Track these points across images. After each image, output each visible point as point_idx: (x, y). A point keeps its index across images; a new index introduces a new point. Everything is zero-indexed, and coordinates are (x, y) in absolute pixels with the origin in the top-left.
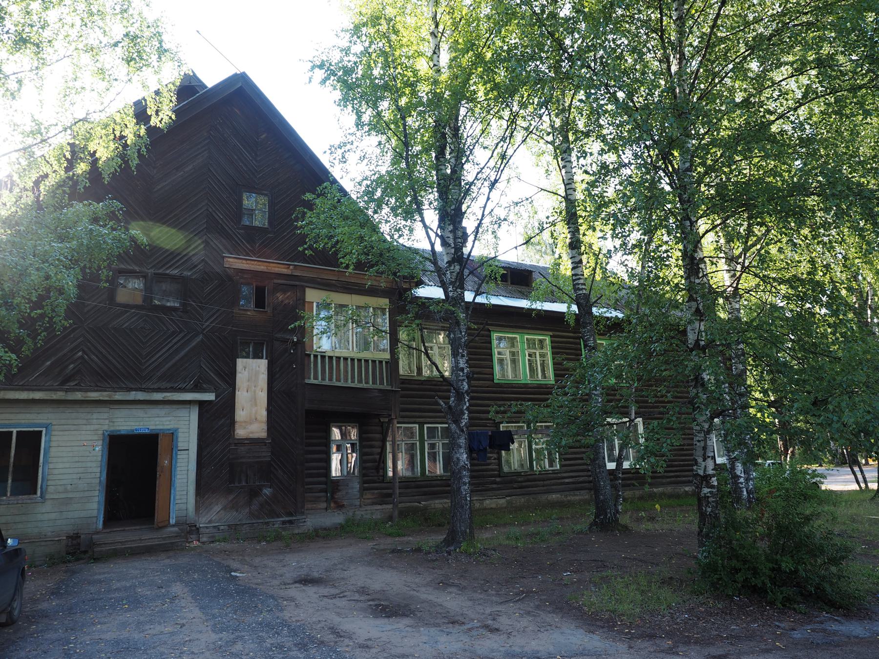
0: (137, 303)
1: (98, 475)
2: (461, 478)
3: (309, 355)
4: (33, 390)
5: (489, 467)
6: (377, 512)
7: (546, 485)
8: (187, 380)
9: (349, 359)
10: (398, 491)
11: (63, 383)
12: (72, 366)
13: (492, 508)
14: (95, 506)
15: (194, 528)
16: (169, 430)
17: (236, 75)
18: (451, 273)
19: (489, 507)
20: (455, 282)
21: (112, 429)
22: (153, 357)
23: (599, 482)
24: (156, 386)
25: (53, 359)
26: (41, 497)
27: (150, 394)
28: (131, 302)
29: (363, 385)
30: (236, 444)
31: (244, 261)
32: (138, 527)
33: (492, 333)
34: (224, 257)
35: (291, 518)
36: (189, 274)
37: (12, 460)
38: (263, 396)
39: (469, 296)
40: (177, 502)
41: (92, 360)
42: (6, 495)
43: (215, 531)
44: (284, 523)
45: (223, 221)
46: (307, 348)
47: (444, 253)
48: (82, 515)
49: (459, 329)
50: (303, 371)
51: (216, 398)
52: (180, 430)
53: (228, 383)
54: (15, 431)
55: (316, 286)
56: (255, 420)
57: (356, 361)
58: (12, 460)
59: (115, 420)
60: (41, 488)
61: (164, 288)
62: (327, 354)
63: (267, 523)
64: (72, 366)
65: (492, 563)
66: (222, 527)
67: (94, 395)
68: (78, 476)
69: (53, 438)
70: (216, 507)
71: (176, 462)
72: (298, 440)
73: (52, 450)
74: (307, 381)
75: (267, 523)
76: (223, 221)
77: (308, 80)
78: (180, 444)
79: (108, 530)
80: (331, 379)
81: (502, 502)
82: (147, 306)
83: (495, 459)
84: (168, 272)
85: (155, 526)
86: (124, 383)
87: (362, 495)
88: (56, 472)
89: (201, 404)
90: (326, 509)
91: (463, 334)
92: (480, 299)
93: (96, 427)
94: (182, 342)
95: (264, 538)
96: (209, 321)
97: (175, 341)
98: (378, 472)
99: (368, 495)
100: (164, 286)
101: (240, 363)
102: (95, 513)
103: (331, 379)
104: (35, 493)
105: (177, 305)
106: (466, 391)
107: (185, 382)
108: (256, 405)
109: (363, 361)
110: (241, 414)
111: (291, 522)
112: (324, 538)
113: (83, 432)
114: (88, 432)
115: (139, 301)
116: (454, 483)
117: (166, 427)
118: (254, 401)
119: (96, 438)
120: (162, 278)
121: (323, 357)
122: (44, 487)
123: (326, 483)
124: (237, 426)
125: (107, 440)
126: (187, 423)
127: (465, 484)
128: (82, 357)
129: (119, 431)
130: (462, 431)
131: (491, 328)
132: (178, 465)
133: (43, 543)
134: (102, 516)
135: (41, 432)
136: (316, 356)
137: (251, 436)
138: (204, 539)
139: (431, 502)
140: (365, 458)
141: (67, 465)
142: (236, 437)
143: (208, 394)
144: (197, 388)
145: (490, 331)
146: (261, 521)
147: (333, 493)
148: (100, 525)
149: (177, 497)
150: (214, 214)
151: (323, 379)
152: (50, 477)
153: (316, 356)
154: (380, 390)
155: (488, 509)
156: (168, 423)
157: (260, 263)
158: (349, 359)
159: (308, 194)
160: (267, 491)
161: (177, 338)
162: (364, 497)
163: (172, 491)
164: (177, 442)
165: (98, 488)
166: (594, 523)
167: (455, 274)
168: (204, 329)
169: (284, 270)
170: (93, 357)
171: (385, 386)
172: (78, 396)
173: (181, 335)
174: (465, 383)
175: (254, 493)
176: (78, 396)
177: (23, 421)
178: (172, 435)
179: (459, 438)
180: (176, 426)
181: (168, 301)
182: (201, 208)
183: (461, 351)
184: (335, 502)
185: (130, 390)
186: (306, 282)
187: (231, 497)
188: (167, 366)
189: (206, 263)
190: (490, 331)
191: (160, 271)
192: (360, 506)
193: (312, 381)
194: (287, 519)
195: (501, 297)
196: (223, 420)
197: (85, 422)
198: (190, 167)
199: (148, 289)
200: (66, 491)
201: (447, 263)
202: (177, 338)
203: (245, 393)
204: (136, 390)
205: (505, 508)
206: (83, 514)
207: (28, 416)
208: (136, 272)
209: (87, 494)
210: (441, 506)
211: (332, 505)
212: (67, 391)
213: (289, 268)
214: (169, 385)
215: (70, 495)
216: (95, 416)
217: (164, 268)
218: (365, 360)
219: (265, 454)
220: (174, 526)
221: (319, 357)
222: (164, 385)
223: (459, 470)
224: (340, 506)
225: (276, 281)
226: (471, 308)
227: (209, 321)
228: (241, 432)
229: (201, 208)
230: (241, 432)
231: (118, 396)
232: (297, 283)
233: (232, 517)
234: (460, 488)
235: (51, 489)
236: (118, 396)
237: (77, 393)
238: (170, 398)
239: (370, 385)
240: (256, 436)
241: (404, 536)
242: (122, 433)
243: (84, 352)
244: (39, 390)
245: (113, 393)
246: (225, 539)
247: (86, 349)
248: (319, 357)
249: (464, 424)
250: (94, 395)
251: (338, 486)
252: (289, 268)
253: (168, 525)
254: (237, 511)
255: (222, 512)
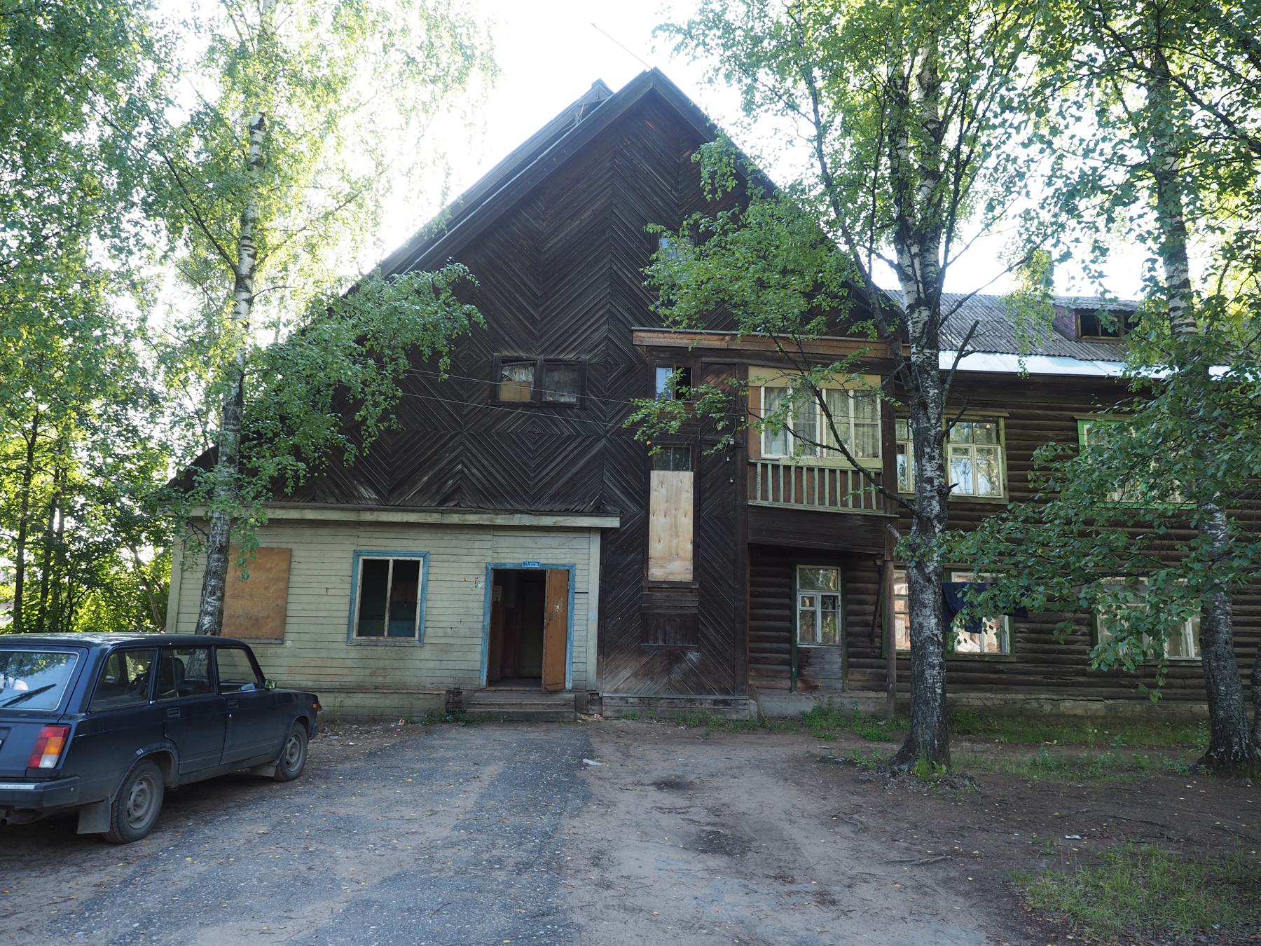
0: (524, 400)
1: (481, 618)
2: (924, 656)
3: (755, 465)
4: (407, 511)
5: (1072, 647)
6: (867, 702)
7: (1190, 687)
8: (587, 500)
9: (816, 470)
10: (894, 673)
11: (442, 503)
12: (450, 482)
13: (1075, 716)
14: (478, 657)
15: (596, 697)
16: (563, 565)
17: (644, 74)
18: (914, 323)
19: (1070, 712)
20: (921, 337)
21: (497, 561)
22: (543, 470)
23: (1217, 685)
24: (547, 508)
25: (431, 474)
26: (420, 640)
27: (537, 518)
28: (517, 399)
29: (838, 509)
30: (650, 589)
31: (660, 335)
32: (527, 689)
33: (1080, 424)
34: (633, 331)
35: (726, 697)
36: (588, 357)
37: (389, 594)
38: (687, 523)
39: (946, 360)
40: (574, 660)
41: (473, 474)
42: (383, 635)
43: (622, 703)
44: (716, 702)
45: (632, 281)
46: (751, 453)
47: (904, 293)
48: (463, 667)
49: (926, 414)
50: (743, 490)
51: (622, 524)
52: (577, 567)
53: (640, 505)
54: (391, 559)
55: (763, 363)
56: (676, 556)
57: (827, 472)
58: (389, 594)
59: (499, 551)
60: (420, 630)
61: (557, 379)
62: (780, 463)
63: (692, 701)
64: (450, 482)
65: (953, 800)
66: (631, 700)
67: (473, 519)
68: (459, 618)
69: (432, 571)
70: (625, 672)
71: (573, 608)
72: (737, 586)
73: (431, 584)
74: (751, 502)
75: (692, 701)
76: (632, 281)
77: (650, 50)
78: (577, 585)
79: (493, 689)
80: (787, 500)
81: (1097, 707)
82: (538, 404)
83: (1084, 634)
84: (561, 357)
85: (542, 688)
86: (508, 502)
87: (845, 675)
88: (435, 611)
89: (604, 532)
90: (790, 690)
91: (933, 422)
92: (968, 364)
93: (478, 558)
94: (579, 449)
95: (685, 720)
96: (614, 421)
97: (569, 449)
98: (872, 641)
99: (857, 676)
100: (557, 376)
101: (655, 476)
102: (477, 665)
103: (787, 500)
104: (414, 636)
105: (573, 400)
106: (937, 516)
107: (584, 503)
108: (677, 536)
109: (838, 472)
110: (656, 548)
111: (725, 703)
112: (771, 731)
113: (464, 565)
114: (469, 565)
115: (527, 398)
116: (914, 663)
117: (560, 562)
118: (675, 529)
119: (478, 572)
120: (553, 365)
121: (775, 467)
122: (422, 629)
123: (790, 653)
124: (651, 562)
125: (491, 575)
126: (586, 557)
127: (932, 666)
128: (461, 471)
129: (505, 564)
130: (929, 580)
131: (1076, 415)
132: (576, 612)
133: (421, 696)
134: (485, 670)
135: (419, 562)
136: (765, 466)
137: (671, 578)
138: (609, 713)
139: (962, 695)
140: (851, 618)
141: (446, 604)
142: (651, 578)
143: (610, 519)
144: (599, 511)
145: (1076, 421)
146: (684, 697)
147: (801, 667)
148: (484, 682)
149: (575, 654)
150: (620, 273)
151: (776, 499)
152: (429, 618)
153: (765, 466)
154: (865, 517)
155: (1069, 716)
156: (562, 556)
157: (682, 336)
158: (816, 470)
159: (650, 225)
160: (693, 656)
161: (573, 445)
162: (850, 677)
163: (568, 646)
164: (574, 582)
165: (480, 635)
166: (1207, 760)
167: (920, 325)
168: (607, 432)
169: (717, 343)
170: (474, 471)
171: (874, 511)
172: (455, 519)
173: (578, 440)
174: (934, 503)
175: (674, 657)
176: (455, 519)
177: (399, 549)
178: (566, 573)
179: (922, 592)
180: (572, 561)
181: (562, 396)
182: (602, 268)
183: (928, 450)
184: (804, 681)
185: (514, 512)
186: (749, 357)
187: (645, 660)
188: (561, 482)
189: (610, 340)
190: (1076, 421)
191: (552, 357)
192: (843, 690)
193: (759, 502)
194: (721, 697)
195: (1099, 363)
196: (633, 555)
197: (465, 551)
198: (588, 213)
199: (538, 382)
200: (445, 636)
201: (908, 307)
202: (573, 445)
203: (662, 519)
204: (521, 512)
205: (1103, 717)
206: (465, 666)
207: (405, 542)
208: (522, 360)
209: (469, 641)
210: (979, 703)
211: (799, 684)
212: (442, 513)
213: (723, 339)
214: (563, 507)
215: (450, 641)
216: (477, 544)
217: (557, 352)
218: (841, 471)
219: (690, 604)
220: (570, 691)
221: (770, 467)
222: (558, 506)
223: (923, 644)
224: (811, 688)
225: (705, 359)
226: (950, 379)
227: (614, 421)
228: (657, 572)
229: (602, 268)
230: (657, 572)
231: (501, 520)
232: (736, 360)
233: (645, 687)
234: (923, 672)
235: (429, 631)
236: (501, 520)
237: (454, 515)
238: (563, 524)
239: (850, 509)
240: (677, 578)
241: (889, 741)
242: (508, 567)
243: (464, 465)
244: (413, 511)
245: (495, 517)
246: (634, 715)
247: (466, 461)
248: (770, 467)
249: (931, 568)
250: (473, 519)
251: (809, 657)
252: (723, 339)
253: (563, 690)
254: (652, 679)
255: (632, 679)
